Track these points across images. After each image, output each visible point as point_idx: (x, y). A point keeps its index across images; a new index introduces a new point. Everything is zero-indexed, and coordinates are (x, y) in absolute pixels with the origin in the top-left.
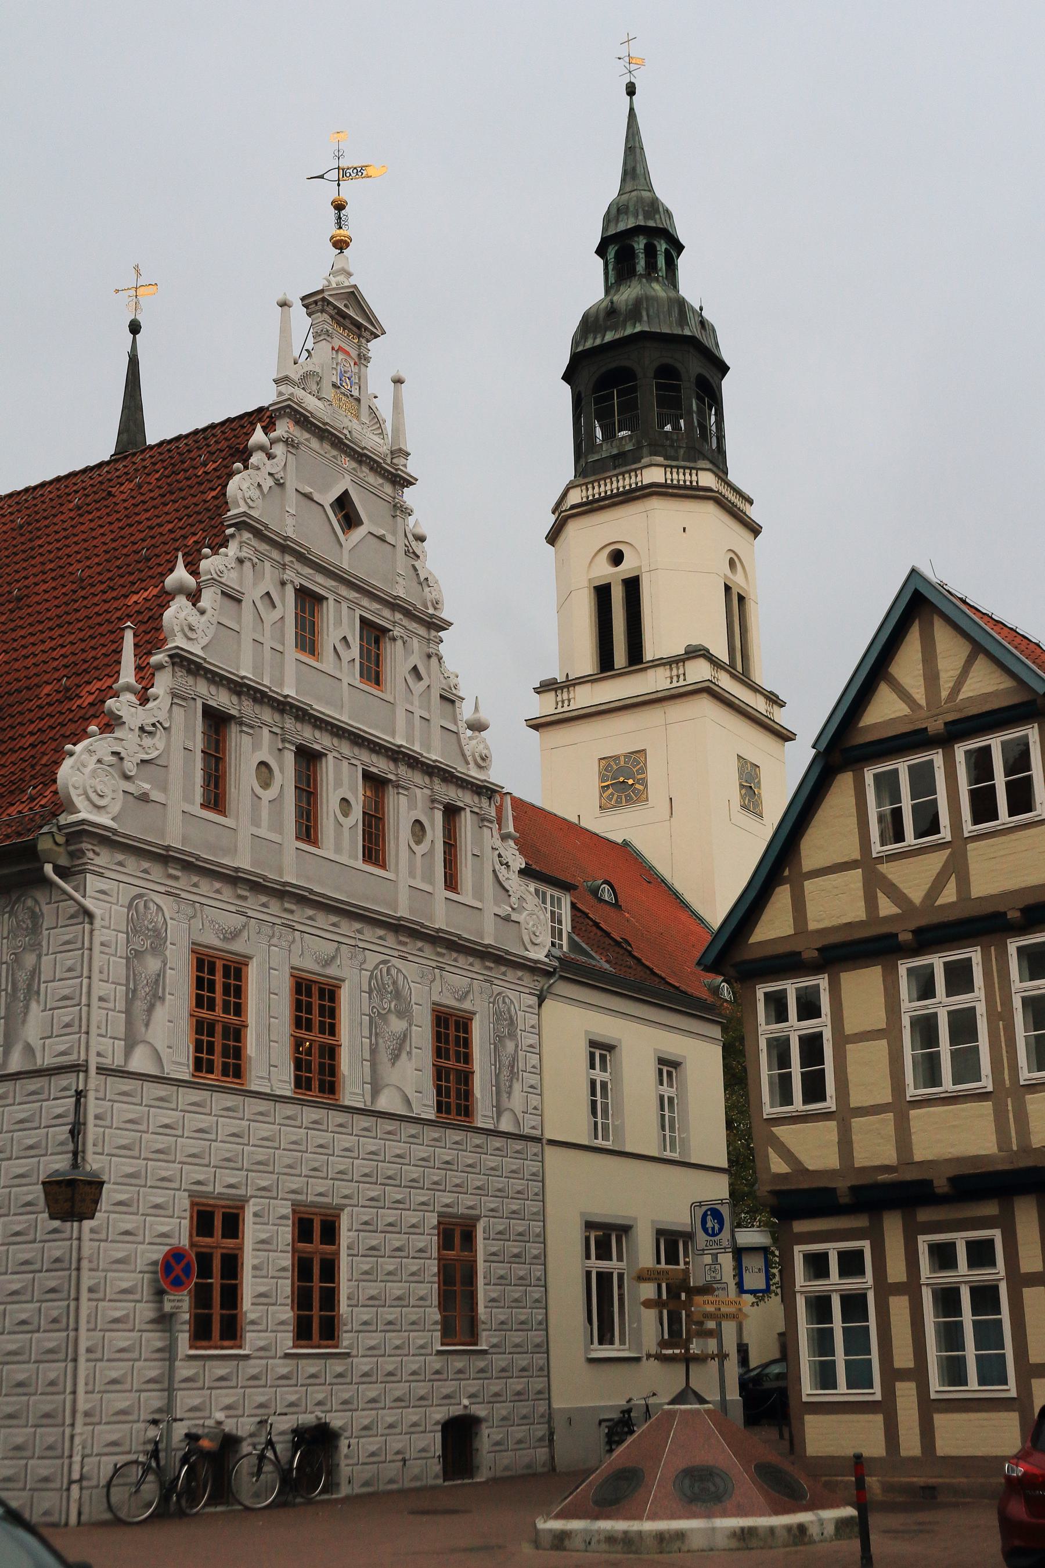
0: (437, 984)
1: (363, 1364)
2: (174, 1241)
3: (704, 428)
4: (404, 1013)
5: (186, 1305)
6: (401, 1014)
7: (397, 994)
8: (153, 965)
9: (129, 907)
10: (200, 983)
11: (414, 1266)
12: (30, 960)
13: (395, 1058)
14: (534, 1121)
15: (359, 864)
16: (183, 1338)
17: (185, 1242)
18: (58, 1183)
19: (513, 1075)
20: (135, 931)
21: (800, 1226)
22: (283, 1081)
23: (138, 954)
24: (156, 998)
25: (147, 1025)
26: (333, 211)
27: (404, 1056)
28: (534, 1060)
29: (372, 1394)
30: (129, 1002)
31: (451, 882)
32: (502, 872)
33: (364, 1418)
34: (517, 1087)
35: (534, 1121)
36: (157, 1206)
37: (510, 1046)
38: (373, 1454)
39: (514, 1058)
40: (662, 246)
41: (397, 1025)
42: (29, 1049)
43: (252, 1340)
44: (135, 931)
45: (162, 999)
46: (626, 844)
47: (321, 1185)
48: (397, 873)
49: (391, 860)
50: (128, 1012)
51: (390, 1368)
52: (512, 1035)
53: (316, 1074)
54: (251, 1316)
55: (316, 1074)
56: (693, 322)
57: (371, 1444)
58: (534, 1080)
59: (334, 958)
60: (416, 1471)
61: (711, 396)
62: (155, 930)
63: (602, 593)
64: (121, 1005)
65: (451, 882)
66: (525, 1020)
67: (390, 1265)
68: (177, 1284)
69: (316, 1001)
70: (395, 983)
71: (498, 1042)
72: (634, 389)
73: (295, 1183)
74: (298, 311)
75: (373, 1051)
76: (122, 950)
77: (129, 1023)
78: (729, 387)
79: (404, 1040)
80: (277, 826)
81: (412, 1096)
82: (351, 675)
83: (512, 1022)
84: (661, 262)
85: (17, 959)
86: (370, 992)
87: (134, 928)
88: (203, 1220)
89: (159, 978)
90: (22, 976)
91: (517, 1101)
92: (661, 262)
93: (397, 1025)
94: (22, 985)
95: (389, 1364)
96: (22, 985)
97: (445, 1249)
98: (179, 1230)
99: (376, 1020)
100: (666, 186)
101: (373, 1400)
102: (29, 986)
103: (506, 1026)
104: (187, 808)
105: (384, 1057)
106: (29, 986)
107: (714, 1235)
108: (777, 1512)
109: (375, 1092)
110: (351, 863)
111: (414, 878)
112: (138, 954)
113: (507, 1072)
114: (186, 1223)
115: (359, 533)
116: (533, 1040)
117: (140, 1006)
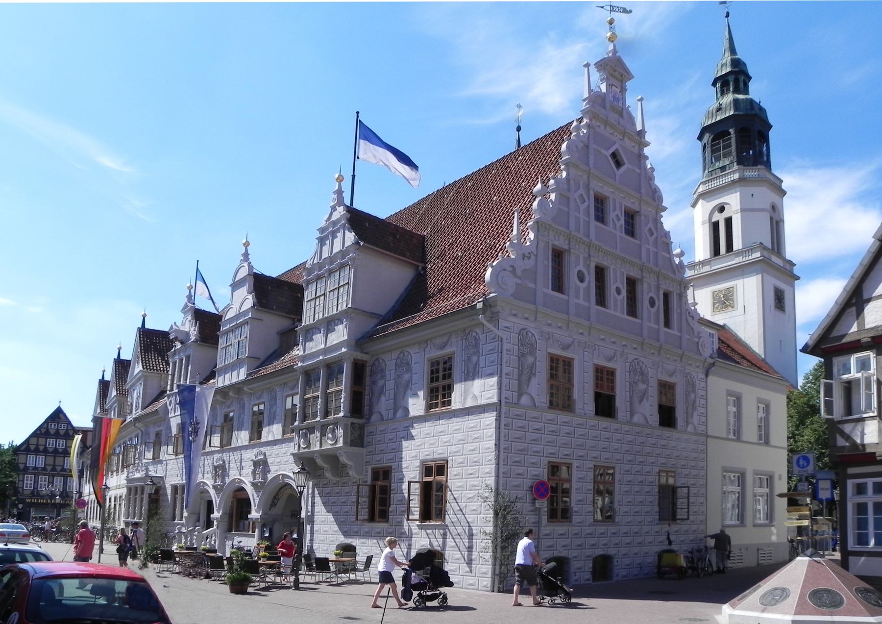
0: (660, 370)
1: (625, 529)
2: (541, 478)
3: (761, 153)
4: (645, 381)
5: (546, 505)
6: (643, 382)
7: (642, 374)
8: (530, 359)
9: (519, 334)
10: (552, 368)
11: (647, 489)
12: (475, 359)
13: (641, 401)
14: (703, 428)
15: (626, 316)
16: (545, 518)
17: (545, 479)
18: (359, 339)
19: (694, 408)
20: (522, 345)
21: (851, 471)
22: (591, 407)
23: (523, 355)
24: (532, 374)
25: (528, 386)
26: (608, 25)
27: (645, 400)
28: (703, 402)
29: (628, 541)
30: (520, 376)
31: (667, 324)
32: (690, 319)
33: (624, 551)
34: (695, 413)
35: (703, 428)
36: (533, 463)
37: (693, 396)
38: (628, 565)
39: (694, 401)
40: (742, 78)
41: (642, 386)
42: (475, 397)
43: (576, 519)
44: (522, 345)
45: (535, 375)
46: (725, 325)
47: (607, 455)
48: (642, 319)
49: (639, 312)
50: (519, 380)
51: (636, 530)
52: (694, 391)
53: (605, 406)
54: (575, 509)
55: (605, 406)
56: (756, 108)
57: (627, 561)
58: (703, 410)
59: (613, 357)
60: (646, 571)
61: (764, 138)
62: (531, 344)
63: (715, 226)
64: (516, 377)
65: (667, 324)
66: (700, 384)
67: (637, 488)
68: (542, 496)
69: (605, 377)
70: (641, 368)
71: (687, 394)
72: (730, 139)
73: (595, 454)
74: (593, 69)
75: (631, 398)
76: (516, 353)
77: (520, 384)
78: (772, 134)
79: (645, 394)
80: (588, 299)
81: (649, 418)
82: (620, 234)
83: (694, 386)
84: (742, 85)
85: (469, 359)
86: (630, 372)
87: (522, 342)
88: (554, 469)
89: (533, 366)
90: (471, 366)
91: (695, 419)
92: (742, 85)
93: (642, 386)
94: (471, 370)
95: (636, 529)
96: (471, 370)
97: (386, 486)
98: (543, 473)
99: (633, 384)
100: (740, 55)
101: (628, 544)
102: (475, 370)
103: (691, 386)
104: (546, 290)
105: (636, 400)
106: (475, 370)
107: (803, 467)
108: (872, 615)
109: (632, 415)
110: (621, 315)
111: (650, 321)
112: (523, 355)
113: (692, 406)
114: (546, 471)
115: (623, 169)
116: (702, 393)
117: (524, 378)
